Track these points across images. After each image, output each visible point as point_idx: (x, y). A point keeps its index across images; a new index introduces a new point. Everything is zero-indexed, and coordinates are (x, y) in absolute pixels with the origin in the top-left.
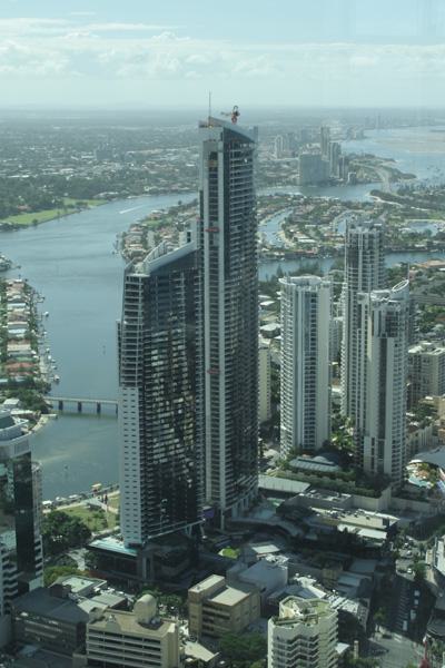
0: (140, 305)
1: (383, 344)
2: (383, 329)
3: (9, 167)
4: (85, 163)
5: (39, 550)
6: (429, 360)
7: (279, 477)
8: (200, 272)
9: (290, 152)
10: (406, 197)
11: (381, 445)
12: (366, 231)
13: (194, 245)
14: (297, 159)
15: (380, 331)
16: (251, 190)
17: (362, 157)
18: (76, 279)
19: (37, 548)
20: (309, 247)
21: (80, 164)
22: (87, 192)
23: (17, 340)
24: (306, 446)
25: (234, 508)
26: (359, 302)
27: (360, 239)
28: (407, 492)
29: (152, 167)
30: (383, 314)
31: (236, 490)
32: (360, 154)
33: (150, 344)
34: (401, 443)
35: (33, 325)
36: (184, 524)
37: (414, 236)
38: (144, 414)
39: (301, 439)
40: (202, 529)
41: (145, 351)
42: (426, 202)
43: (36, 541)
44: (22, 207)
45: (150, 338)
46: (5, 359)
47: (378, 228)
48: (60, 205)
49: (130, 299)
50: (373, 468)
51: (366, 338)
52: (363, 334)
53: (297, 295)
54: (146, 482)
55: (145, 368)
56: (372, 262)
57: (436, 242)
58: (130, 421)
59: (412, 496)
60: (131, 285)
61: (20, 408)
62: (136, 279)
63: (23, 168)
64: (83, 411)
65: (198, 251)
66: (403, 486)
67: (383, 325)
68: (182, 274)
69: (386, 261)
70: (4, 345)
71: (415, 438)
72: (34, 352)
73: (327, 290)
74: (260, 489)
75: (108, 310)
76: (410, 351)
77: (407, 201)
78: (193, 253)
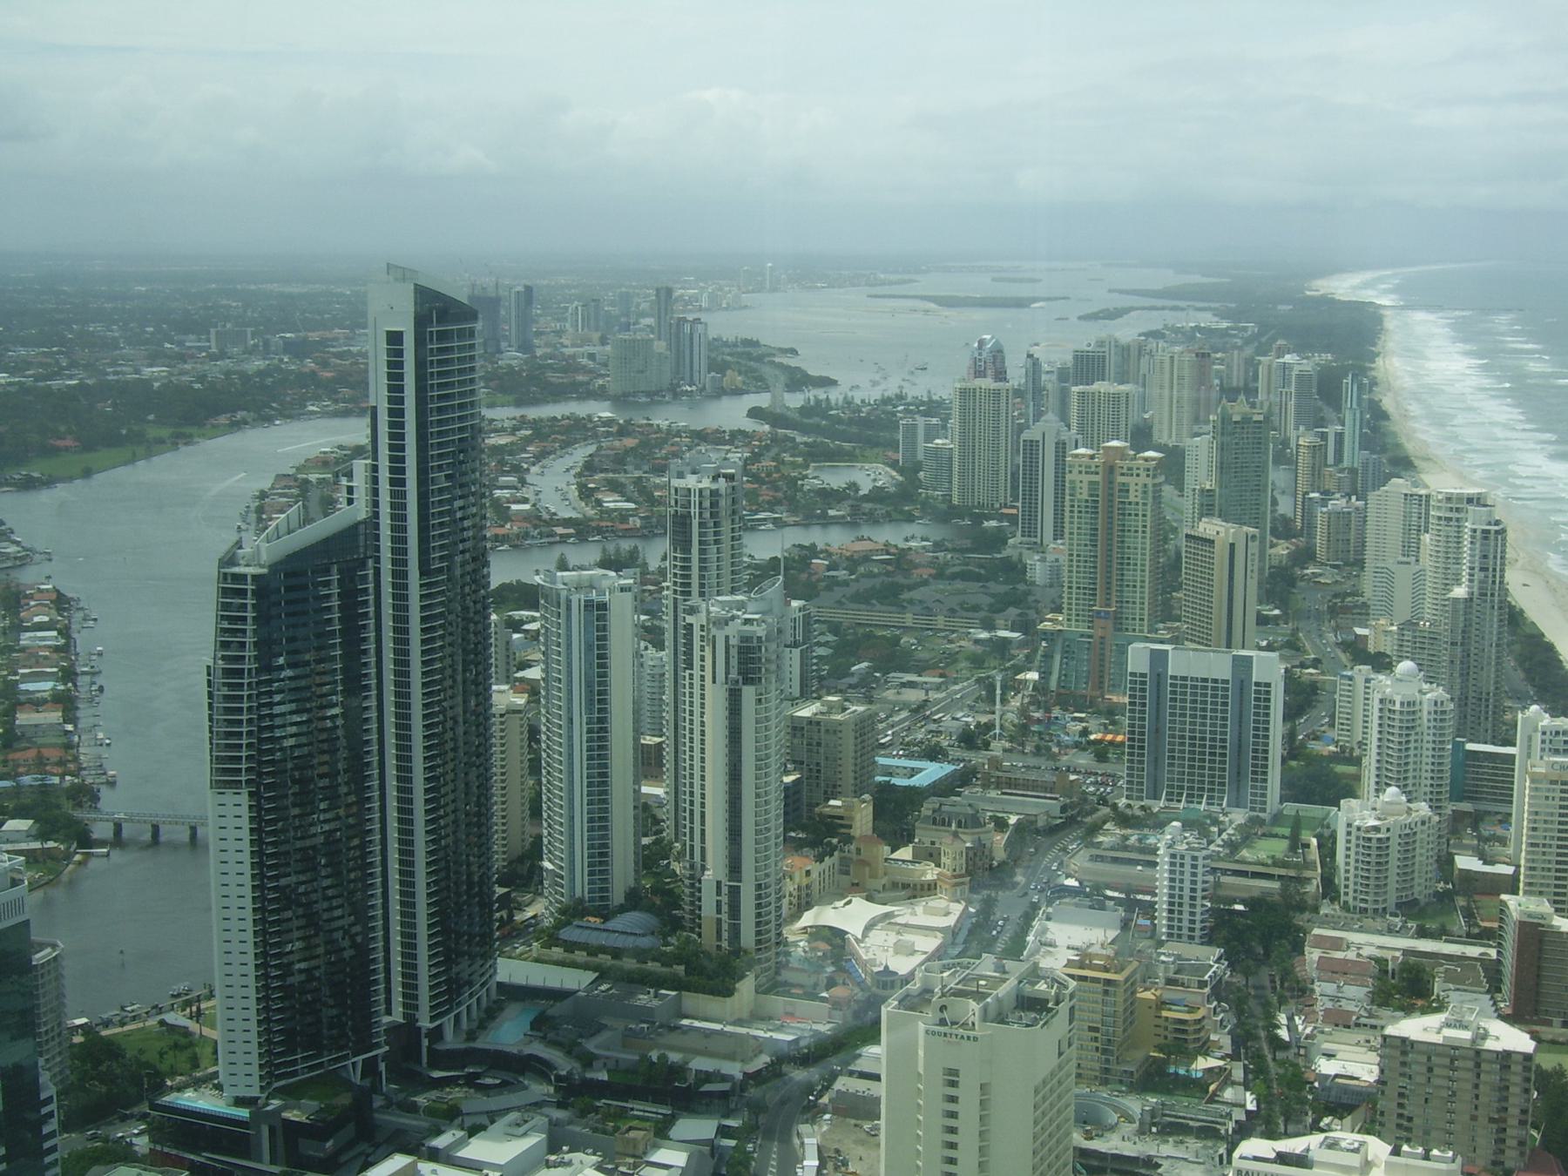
0: (249, 627)
1: (734, 699)
2: (734, 675)
3: (41, 365)
4: (193, 356)
5: (51, 1114)
6: (835, 730)
7: (537, 960)
8: (370, 562)
9: (596, 336)
10: (816, 420)
11: (735, 893)
12: (706, 483)
13: (361, 511)
14: (608, 348)
15: (727, 673)
16: (472, 404)
17: (735, 345)
18: (149, 565)
19: (44, 1111)
20: (624, 516)
21: (183, 358)
22: (197, 411)
23: (37, 704)
24: (591, 900)
25: (448, 1022)
26: (689, 619)
27: (695, 499)
28: (786, 983)
29: (324, 364)
30: (733, 642)
31: (450, 991)
32: (732, 339)
33: (270, 682)
34: (771, 890)
35: (69, 675)
36: (346, 1057)
37: (708, 1077)
38: (266, 976)
39: (582, 888)
40: (382, 1067)
41: (260, 706)
42: (854, 429)
43: (43, 1096)
44: (60, 443)
45: (272, 716)
46: (12, 739)
47: (730, 478)
48: (137, 439)
49: (229, 618)
50: (719, 937)
51: (703, 687)
52: (697, 682)
53: (569, 608)
54: (268, 1041)
55: (261, 741)
56: (716, 542)
57: (867, 506)
58: (232, 857)
59: (881, 510)
60: (231, 587)
61: (36, 838)
62: (240, 578)
63: (72, 365)
64: (163, 838)
65: (364, 522)
66: (777, 973)
67: (734, 662)
68: (335, 568)
69: (745, 541)
70: (10, 713)
71: (805, 881)
72: (70, 727)
73: (628, 596)
74: (500, 984)
75: (193, 639)
76: (645, 789)
77: (817, 430)
78: (356, 526)
